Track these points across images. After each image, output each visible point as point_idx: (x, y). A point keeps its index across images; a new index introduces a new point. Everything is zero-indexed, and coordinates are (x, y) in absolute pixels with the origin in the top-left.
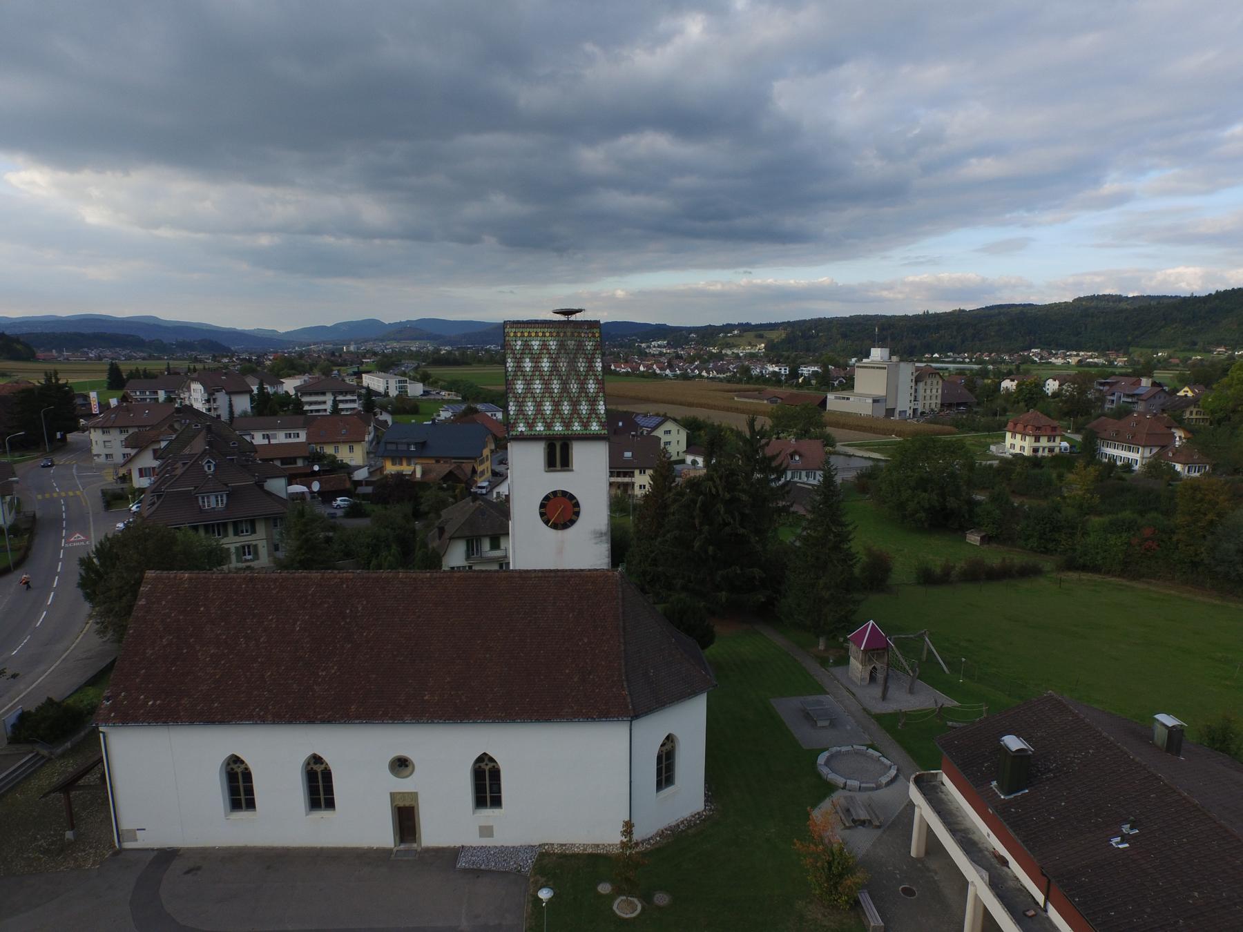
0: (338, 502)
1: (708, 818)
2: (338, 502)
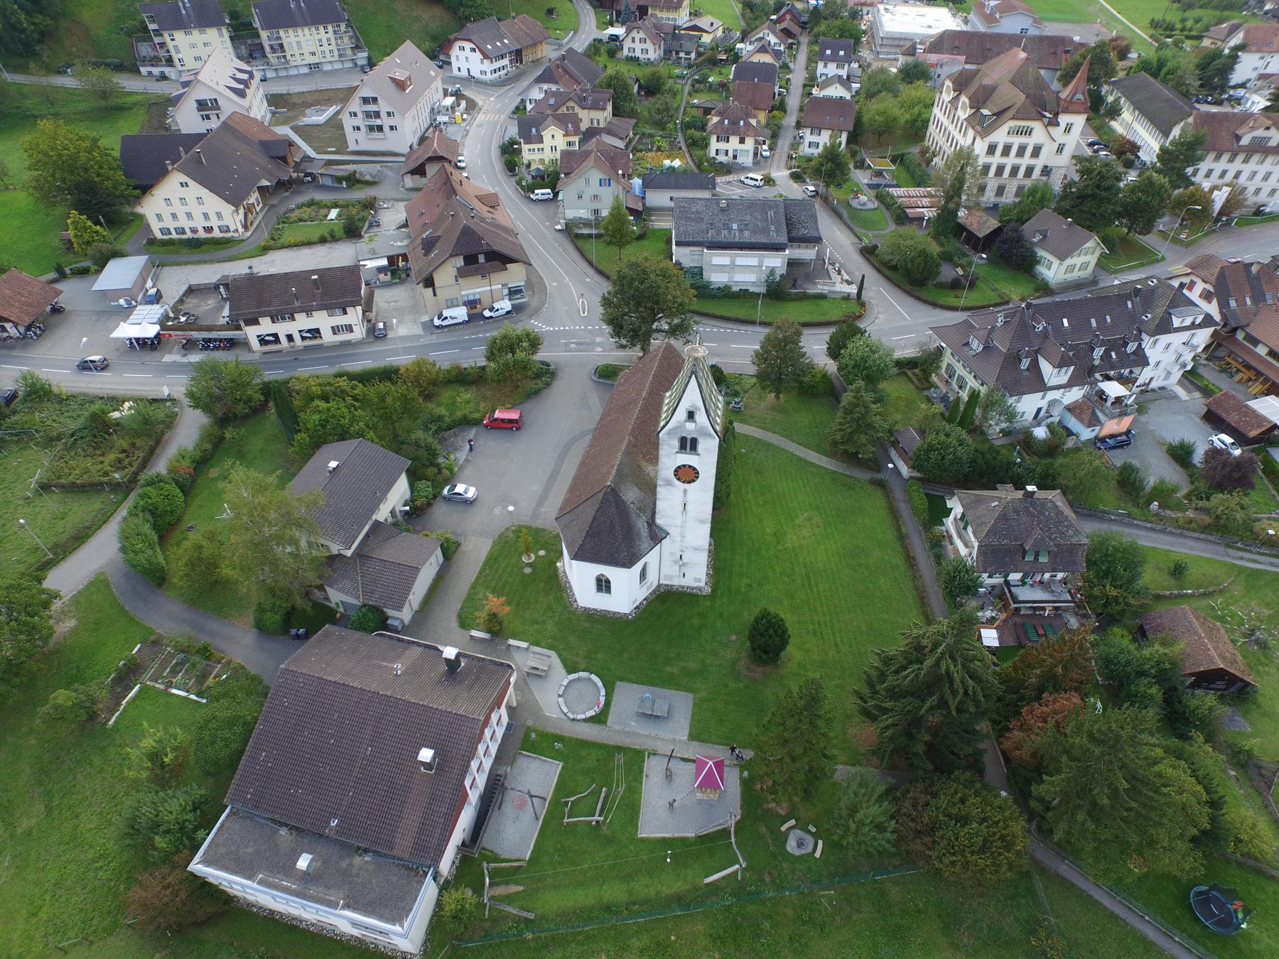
0: (1215, 439)
1: (572, 605)
2: (1215, 439)
